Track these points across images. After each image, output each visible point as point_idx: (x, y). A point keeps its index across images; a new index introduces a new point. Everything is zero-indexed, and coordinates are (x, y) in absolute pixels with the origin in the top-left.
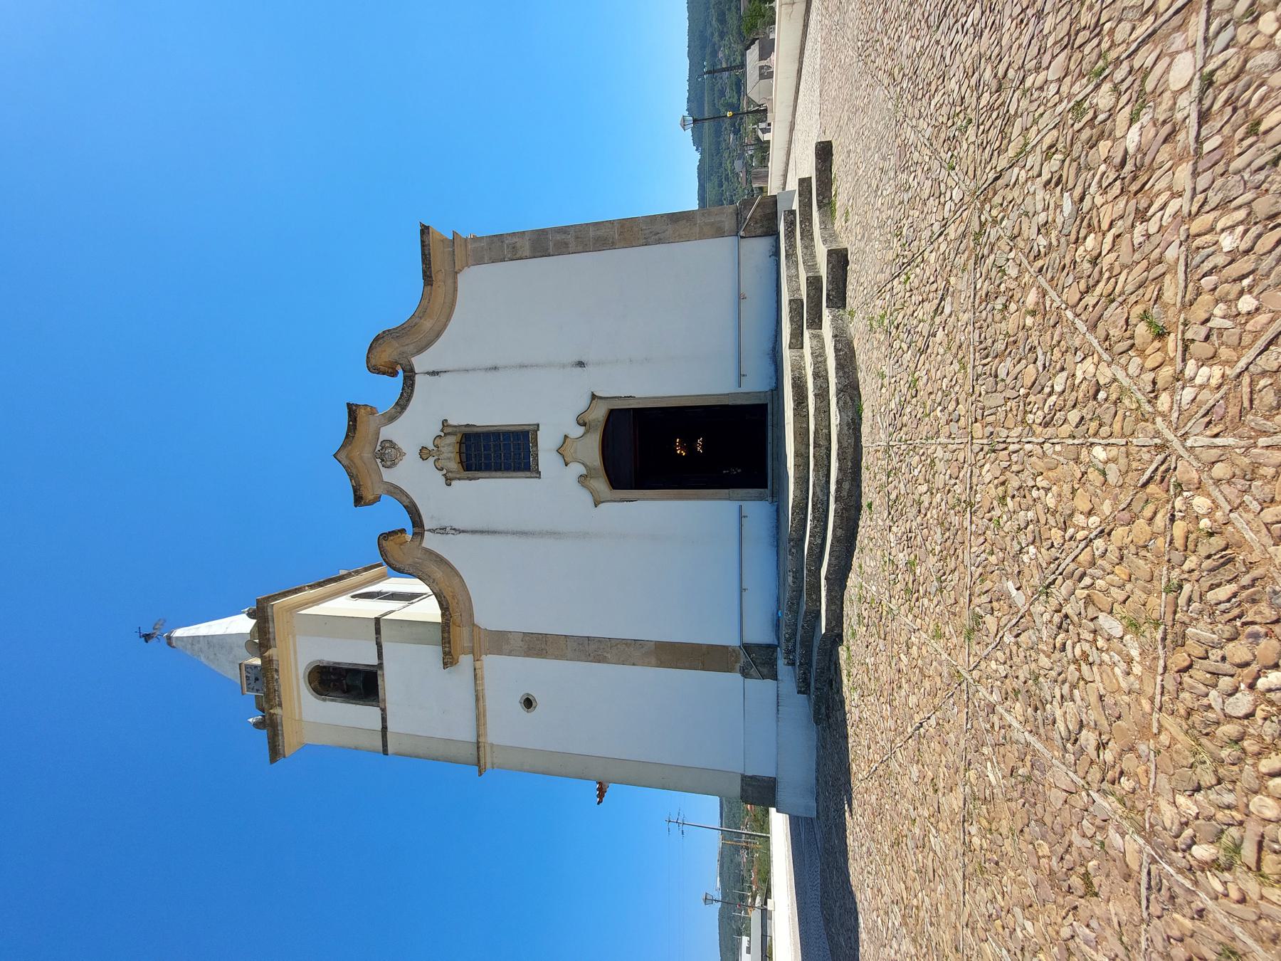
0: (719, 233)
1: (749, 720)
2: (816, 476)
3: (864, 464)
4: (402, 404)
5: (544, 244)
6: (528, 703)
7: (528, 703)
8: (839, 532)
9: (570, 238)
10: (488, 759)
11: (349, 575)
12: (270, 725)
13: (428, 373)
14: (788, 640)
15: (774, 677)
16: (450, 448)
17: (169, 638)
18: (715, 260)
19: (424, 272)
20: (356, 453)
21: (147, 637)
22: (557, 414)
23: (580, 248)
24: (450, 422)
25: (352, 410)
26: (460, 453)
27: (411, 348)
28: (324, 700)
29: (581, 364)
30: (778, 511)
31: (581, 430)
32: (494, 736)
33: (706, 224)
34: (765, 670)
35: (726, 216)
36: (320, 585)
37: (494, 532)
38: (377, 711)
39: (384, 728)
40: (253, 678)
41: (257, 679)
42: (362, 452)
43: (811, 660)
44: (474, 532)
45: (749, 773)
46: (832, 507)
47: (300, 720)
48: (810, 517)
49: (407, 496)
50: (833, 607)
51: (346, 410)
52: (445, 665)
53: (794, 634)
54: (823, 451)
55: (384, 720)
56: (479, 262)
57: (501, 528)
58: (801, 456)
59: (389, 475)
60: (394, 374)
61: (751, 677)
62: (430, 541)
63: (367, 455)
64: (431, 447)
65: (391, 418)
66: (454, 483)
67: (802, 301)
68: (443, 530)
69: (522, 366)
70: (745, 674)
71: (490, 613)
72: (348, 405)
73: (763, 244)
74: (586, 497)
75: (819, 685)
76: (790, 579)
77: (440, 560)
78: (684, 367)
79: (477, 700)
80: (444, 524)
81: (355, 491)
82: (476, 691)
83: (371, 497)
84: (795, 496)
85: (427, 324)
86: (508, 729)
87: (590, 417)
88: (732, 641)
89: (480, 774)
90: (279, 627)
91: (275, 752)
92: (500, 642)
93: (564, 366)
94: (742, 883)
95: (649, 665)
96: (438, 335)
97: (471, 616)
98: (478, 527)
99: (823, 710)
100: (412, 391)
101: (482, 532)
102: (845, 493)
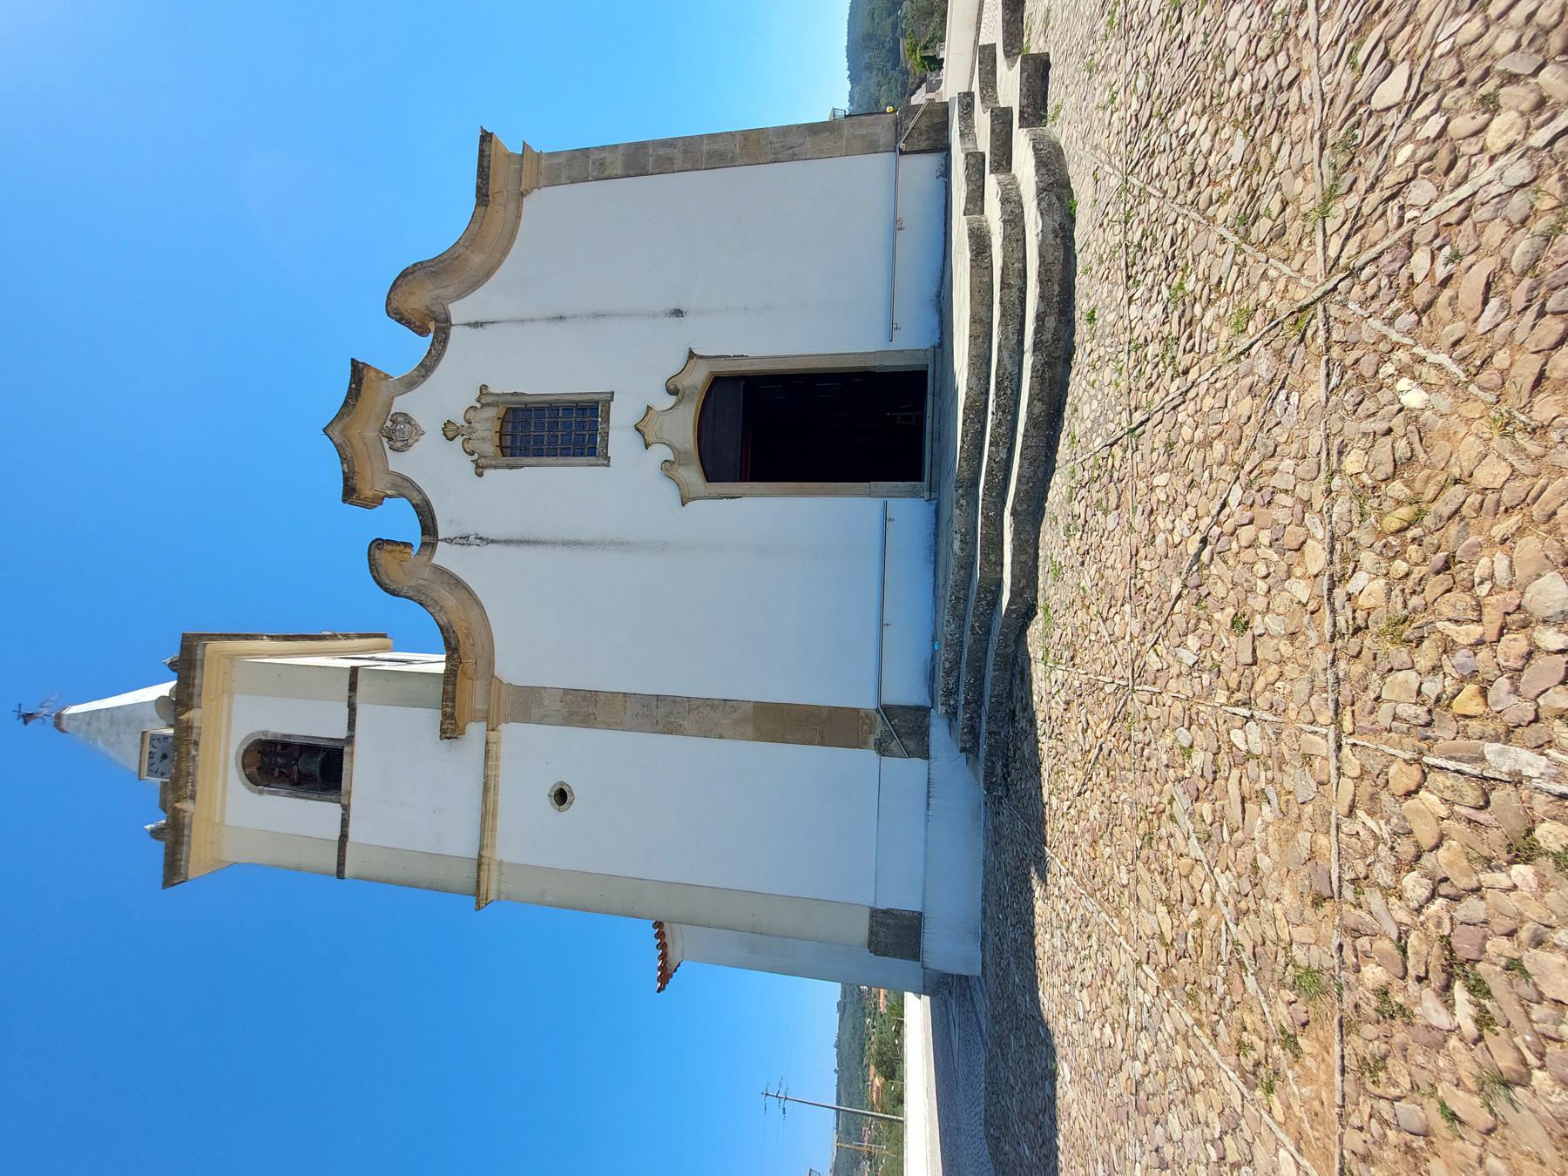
0: (872, 148)
1: (882, 830)
2: (1003, 333)
3: (1082, 305)
4: (427, 367)
5: (642, 160)
6: (561, 796)
7: (561, 796)
8: (1032, 432)
9: (677, 153)
10: (492, 886)
11: (334, 637)
12: (174, 834)
13: (469, 324)
14: (948, 673)
15: (925, 754)
16: (486, 428)
17: (59, 717)
18: (866, 176)
19: (478, 188)
20: (355, 432)
21: (27, 718)
22: (640, 379)
23: (689, 165)
24: (492, 390)
25: (358, 371)
26: (501, 434)
27: (450, 291)
28: (261, 793)
29: (678, 313)
30: (937, 512)
31: (673, 399)
32: (509, 848)
33: (856, 137)
34: (911, 744)
35: (882, 128)
36: (287, 638)
37: (537, 542)
38: (336, 810)
39: (344, 837)
40: (158, 756)
41: (164, 757)
42: (366, 431)
43: (981, 695)
44: (507, 542)
45: (882, 906)
46: (1028, 360)
47: (222, 822)
48: (991, 408)
49: (419, 491)
50: (1023, 558)
51: (349, 368)
52: (443, 731)
53: (956, 663)
54: (1015, 294)
55: (345, 823)
56: (555, 181)
57: (547, 537)
58: (981, 323)
59: (398, 463)
60: (422, 331)
61: (892, 755)
62: (444, 556)
63: (371, 433)
64: (460, 421)
65: (410, 383)
66: (487, 473)
67: (983, 155)
68: (464, 540)
69: (598, 315)
70: (882, 750)
71: (517, 661)
72: (353, 360)
73: (926, 164)
74: (670, 492)
75: (994, 728)
76: (957, 545)
77: (456, 583)
78: (818, 320)
79: (486, 790)
80: (466, 530)
81: (347, 479)
82: (486, 777)
83: (369, 493)
84: (1031, 388)
85: (476, 259)
86: (530, 839)
87: (685, 382)
88: (864, 700)
89: (479, 908)
90: (209, 679)
91: (173, 871)
92: (528, 704)
93: (655, 316)
94: (870, 1055)
95: (743, 737)
96: (489, 274)
97: (491, 663)
98: (515, 535)
99: (999, 770)
100: (444, 347)
101: (519, 542)
102: (1048, 336)
